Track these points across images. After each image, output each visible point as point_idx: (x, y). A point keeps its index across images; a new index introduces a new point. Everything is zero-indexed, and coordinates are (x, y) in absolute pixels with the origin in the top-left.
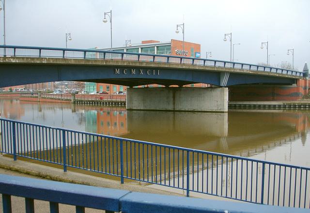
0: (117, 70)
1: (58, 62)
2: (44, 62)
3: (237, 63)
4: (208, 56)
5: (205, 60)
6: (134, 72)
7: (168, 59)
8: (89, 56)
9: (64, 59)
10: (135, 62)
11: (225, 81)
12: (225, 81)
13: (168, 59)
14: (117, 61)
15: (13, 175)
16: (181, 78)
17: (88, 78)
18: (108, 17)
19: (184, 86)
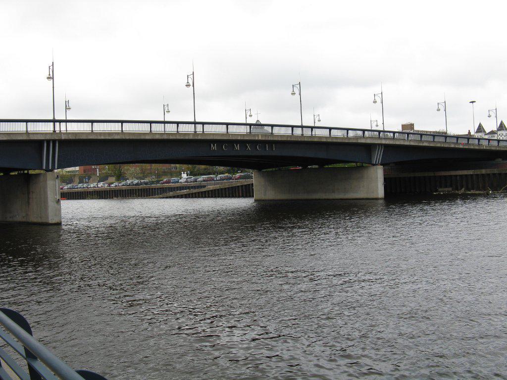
0: (237, 146)
1: (344, 141)
2: (316, 140)
3: (437, 136)
4: (316, 121)
5: (312, 128)
6: (238, 147)
7: (178, 126)
8: (335, 133)
9: (27, 133)
10: (223, 135)
11: (378, 156)
12: (378, 156)
13: (178, 126)
14: (266, 135)
15: (399, 224)
16: (322, 155)
17: (112, 162)
18: (379, 100)
19: (309, 167)
